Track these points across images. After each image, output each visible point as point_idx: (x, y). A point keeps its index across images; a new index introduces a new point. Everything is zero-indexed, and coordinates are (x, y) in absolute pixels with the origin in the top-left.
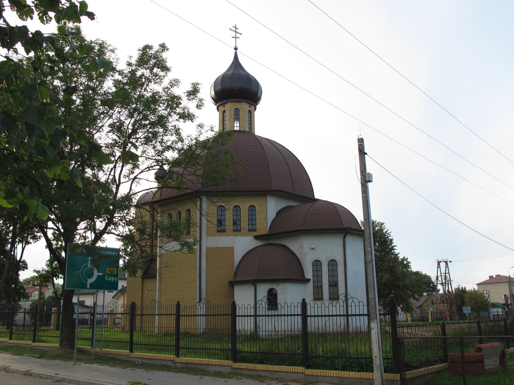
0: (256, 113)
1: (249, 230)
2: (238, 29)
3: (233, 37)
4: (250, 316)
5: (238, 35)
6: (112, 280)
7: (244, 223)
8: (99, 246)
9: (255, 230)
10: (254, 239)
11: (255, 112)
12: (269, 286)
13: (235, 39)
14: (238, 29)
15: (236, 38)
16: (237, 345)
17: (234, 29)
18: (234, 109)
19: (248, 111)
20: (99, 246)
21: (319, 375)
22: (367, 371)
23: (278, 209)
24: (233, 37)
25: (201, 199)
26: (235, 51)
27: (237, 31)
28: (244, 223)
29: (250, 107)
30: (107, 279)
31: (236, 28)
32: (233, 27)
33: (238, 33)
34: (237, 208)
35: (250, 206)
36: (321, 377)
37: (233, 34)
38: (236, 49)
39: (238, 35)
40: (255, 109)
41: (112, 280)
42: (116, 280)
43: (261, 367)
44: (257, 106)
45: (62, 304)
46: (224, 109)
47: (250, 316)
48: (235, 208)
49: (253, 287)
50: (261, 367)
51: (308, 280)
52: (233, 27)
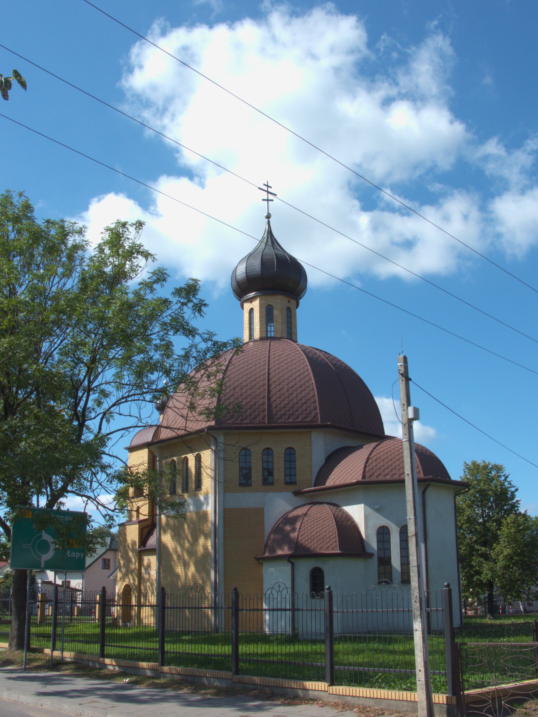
0: (300, 313)
1: (286, 483)
2: (271, 187)
3: (263, 200)
4: (286, 610)
5: (271, 197)
6: (77, 556)
7: (279, 474)
8: (68, 509)
9: (295, 483)
10: (293, 495)
11: (298, 310)
12: (313, 563)
13: (266, 202)
14: (271, 187)
15: (268, 200)
16: (240, 647)
17: (265, 188)
18: (266, 305)
19: (286, 308)
20: (68, 509)
21: (348, 694)
22: (388, 683)
23: (329, 453)
24: (263, 200)
25: (215, 439)
26: (267, 220)
27: (266, 187)
28: (279, 474)
29: (289, 302)
30: (69, 556)
31: (268, 186)
32: (264, 185)
33: (271, 193)
34: (268, 451)
35: (287, 449)
36: (349, 697)
37: (265, 195)
38: (268, 217)
39: (271, 197)
40: (297, 306)
41: (77, 556)
42: (82, 556)
43: (379, 694)
44: (301, 301)
45: (504, 686)
46: (252, 307)
47: (286, 610)
48: (266, 451)
49: (290, 565)
50: (379, 694)
51: (371, 555)
52: (264, 185)
